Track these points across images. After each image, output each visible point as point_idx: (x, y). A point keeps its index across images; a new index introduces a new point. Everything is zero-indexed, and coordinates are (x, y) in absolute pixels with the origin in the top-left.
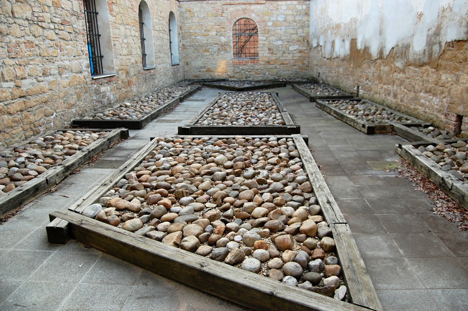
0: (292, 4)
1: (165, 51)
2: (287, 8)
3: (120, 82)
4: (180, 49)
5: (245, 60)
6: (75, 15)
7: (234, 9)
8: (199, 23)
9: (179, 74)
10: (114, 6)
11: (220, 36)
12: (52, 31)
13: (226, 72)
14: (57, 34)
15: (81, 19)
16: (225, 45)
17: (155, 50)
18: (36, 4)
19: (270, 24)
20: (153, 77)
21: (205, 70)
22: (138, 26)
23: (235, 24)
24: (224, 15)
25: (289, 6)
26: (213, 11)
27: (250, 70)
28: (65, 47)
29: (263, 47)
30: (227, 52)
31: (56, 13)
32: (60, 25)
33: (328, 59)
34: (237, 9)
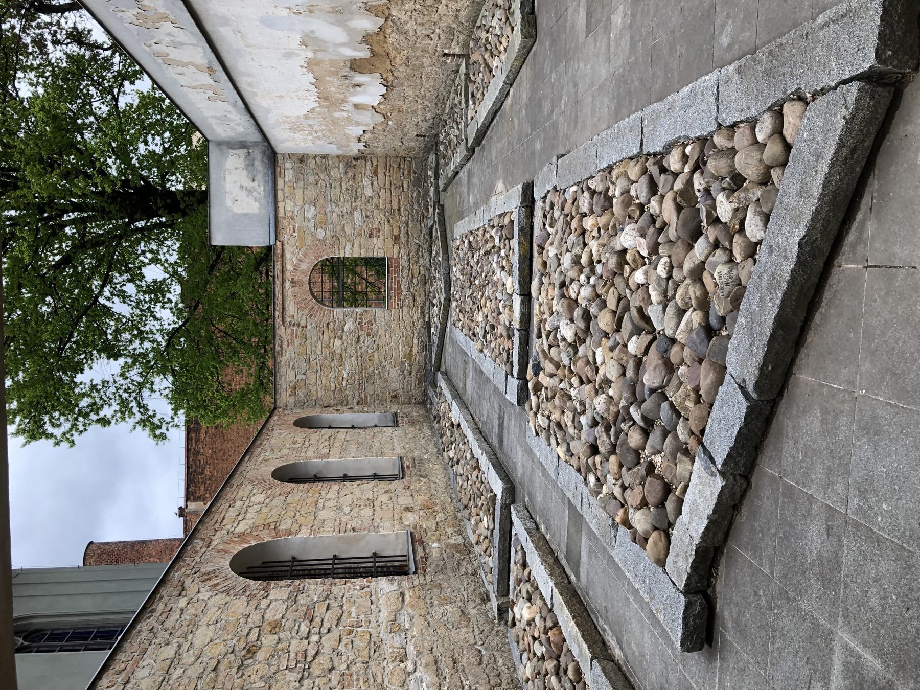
4: (366, 409)
7: (292, 303)
10: (281, 528)
12: (323, 638)
14: (329, 631)
17: (366, 456)
18: (273, 663)
20: (418, 463)
22: (320, 485)
24: (303, 323)
26: (296, 344)
27: (410, 276)
31: (291, 629)
32: (314, 624)
34: (292, 297)
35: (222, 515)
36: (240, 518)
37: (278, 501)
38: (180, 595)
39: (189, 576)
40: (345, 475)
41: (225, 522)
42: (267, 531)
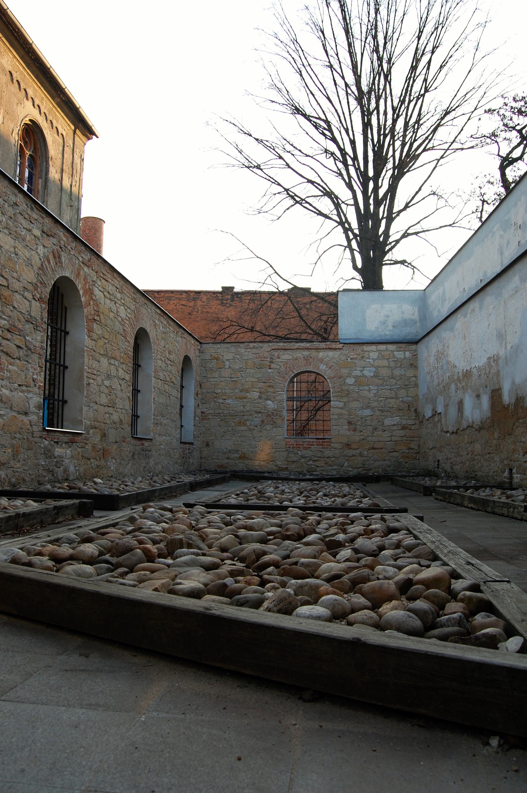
0: (387, 350)
1: (172, 415)
2: (378, 356)
3: (89, 447)
4: (197, 419)
5: (307, 440)
6: (33, 324)
7: (290, 357)
8: (231, 378)
9: (191, 461)
10: (95, 324)
11: (266, 400)
13: (273, 461)
15: (39, 331)
16: (273, 415)
17: (154, 410)
19: (350, 381)
21: (238, 456)
23: (292, 381)
24: (273, 366)
25: (382, 352)
27: (315, 459)
28: (7, 366)
29: (339, 419)
30: (276, 427)
32: (6, 332)
33: (453, 433)
34: (295, 357)
35: (110, 281)
36: (106, 294)
37: (118, 327)
38: (43, 232)
39: (59, 242)
40: (139, 391)
41: (103, 281)
42: (93, 312)
